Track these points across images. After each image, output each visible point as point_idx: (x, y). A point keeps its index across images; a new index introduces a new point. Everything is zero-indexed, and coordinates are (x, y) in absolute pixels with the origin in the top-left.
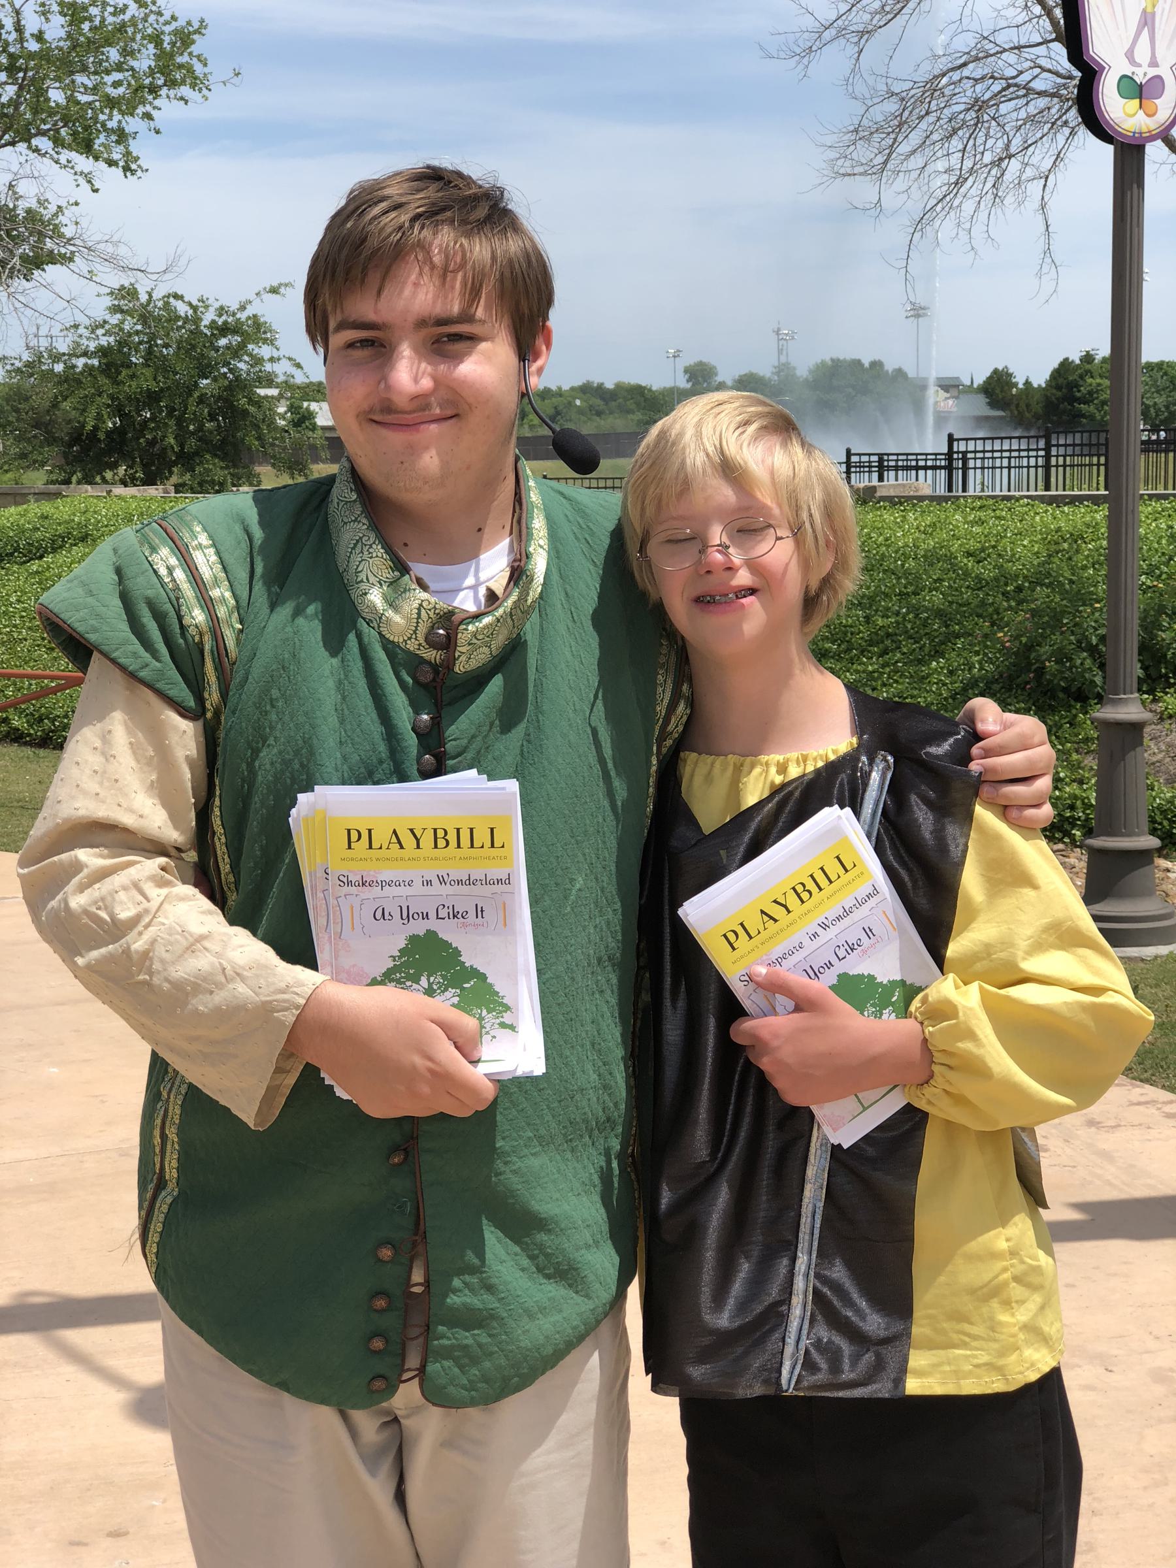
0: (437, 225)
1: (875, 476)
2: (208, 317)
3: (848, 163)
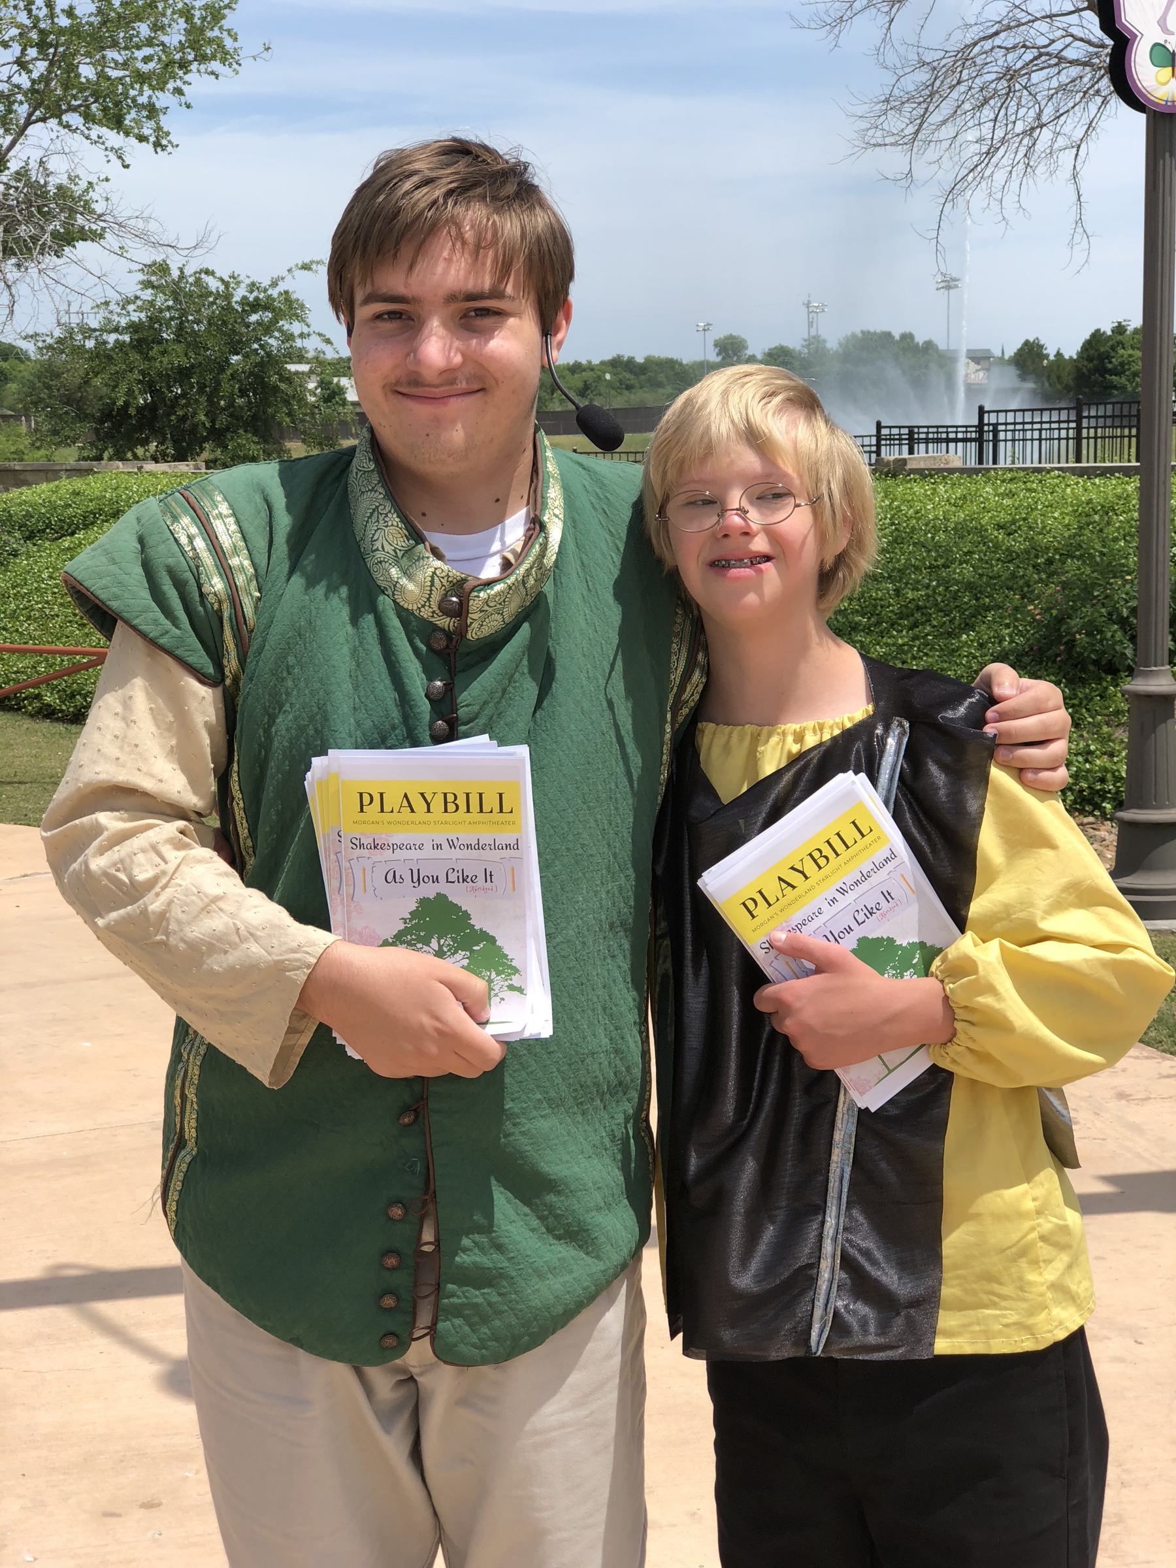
0: (469, 202)
1: (905, 448)
2: (239, 293)
3: (879, 133)
